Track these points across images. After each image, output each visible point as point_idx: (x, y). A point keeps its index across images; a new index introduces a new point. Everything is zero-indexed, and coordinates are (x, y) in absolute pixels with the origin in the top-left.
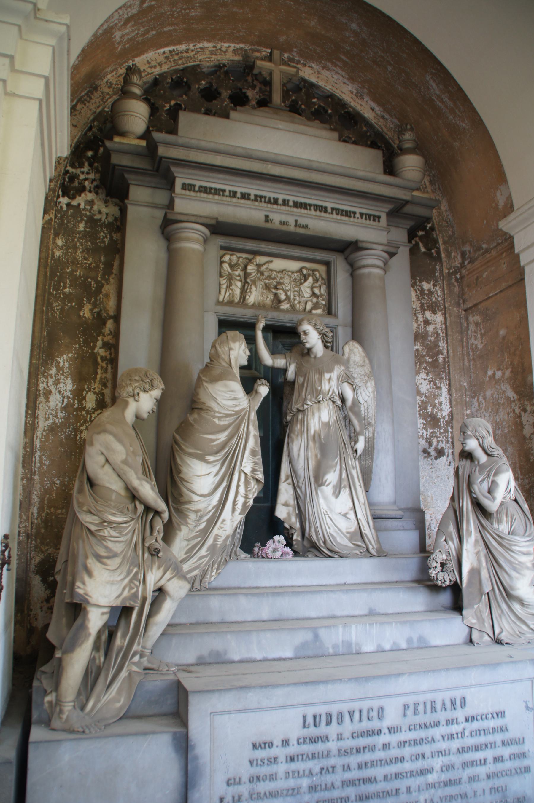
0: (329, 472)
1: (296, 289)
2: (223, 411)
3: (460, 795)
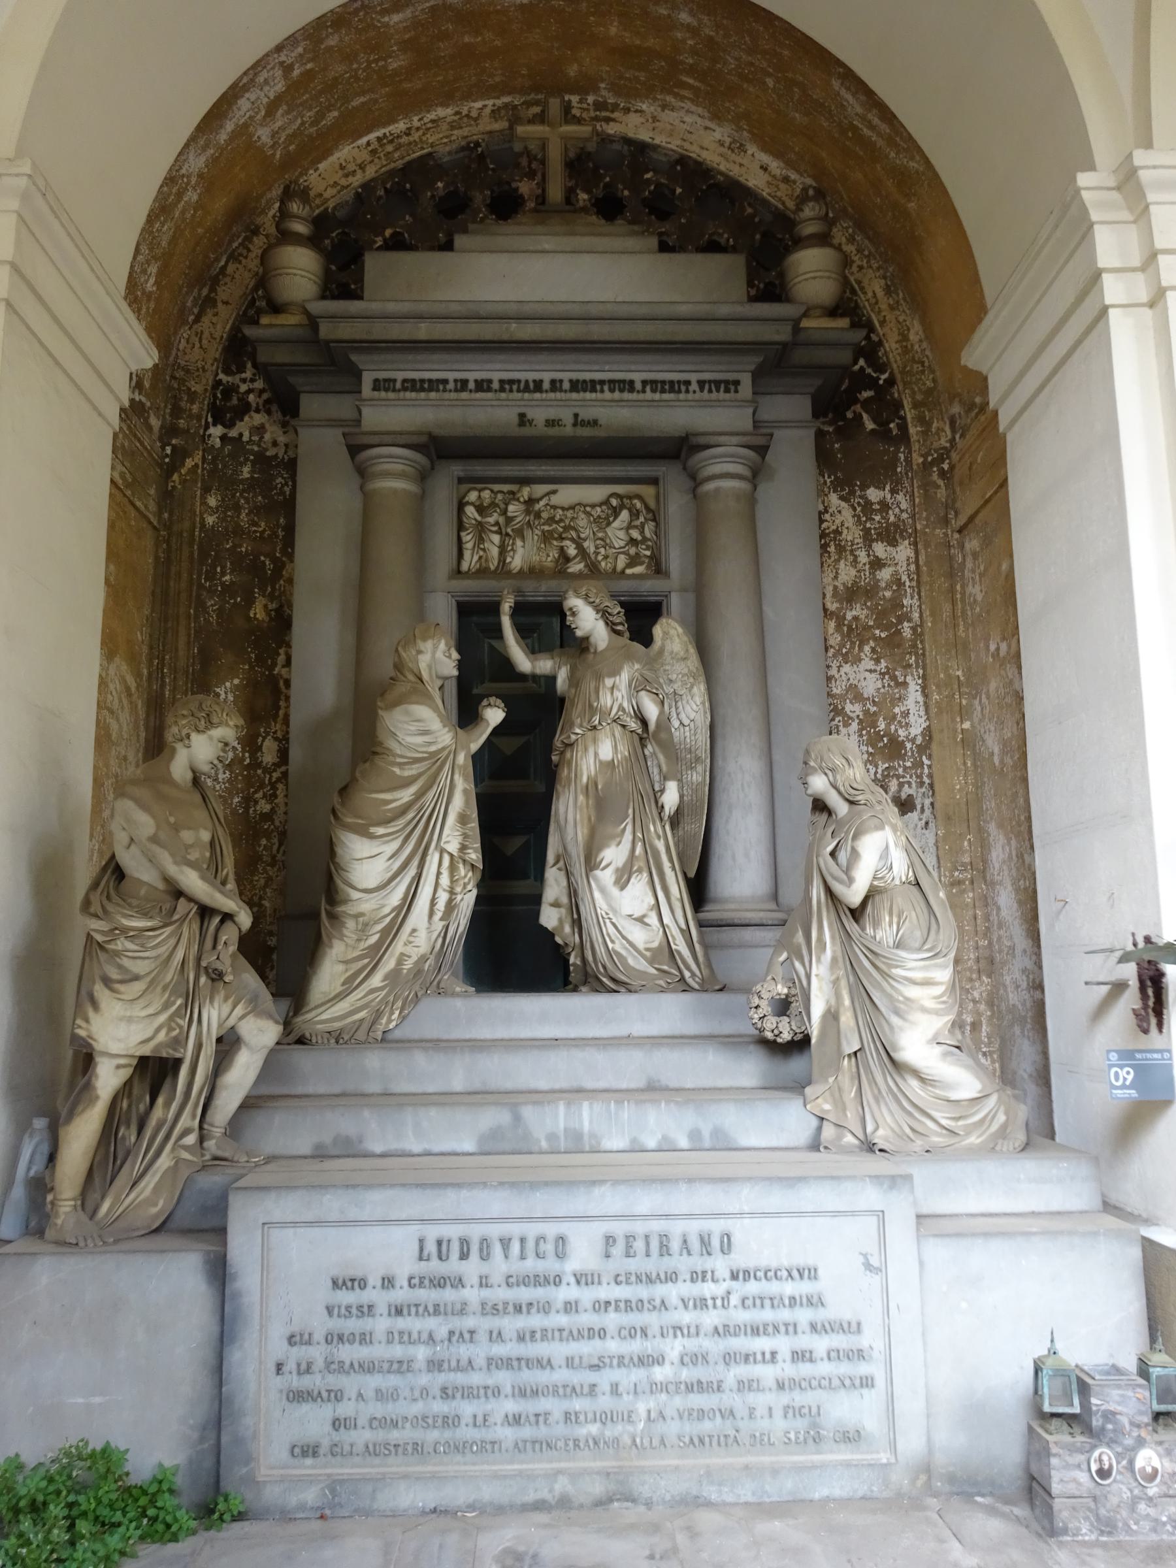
0: (608, 846)
1: (600, 535)
2: (409, 755)
3: (720, 1410)
